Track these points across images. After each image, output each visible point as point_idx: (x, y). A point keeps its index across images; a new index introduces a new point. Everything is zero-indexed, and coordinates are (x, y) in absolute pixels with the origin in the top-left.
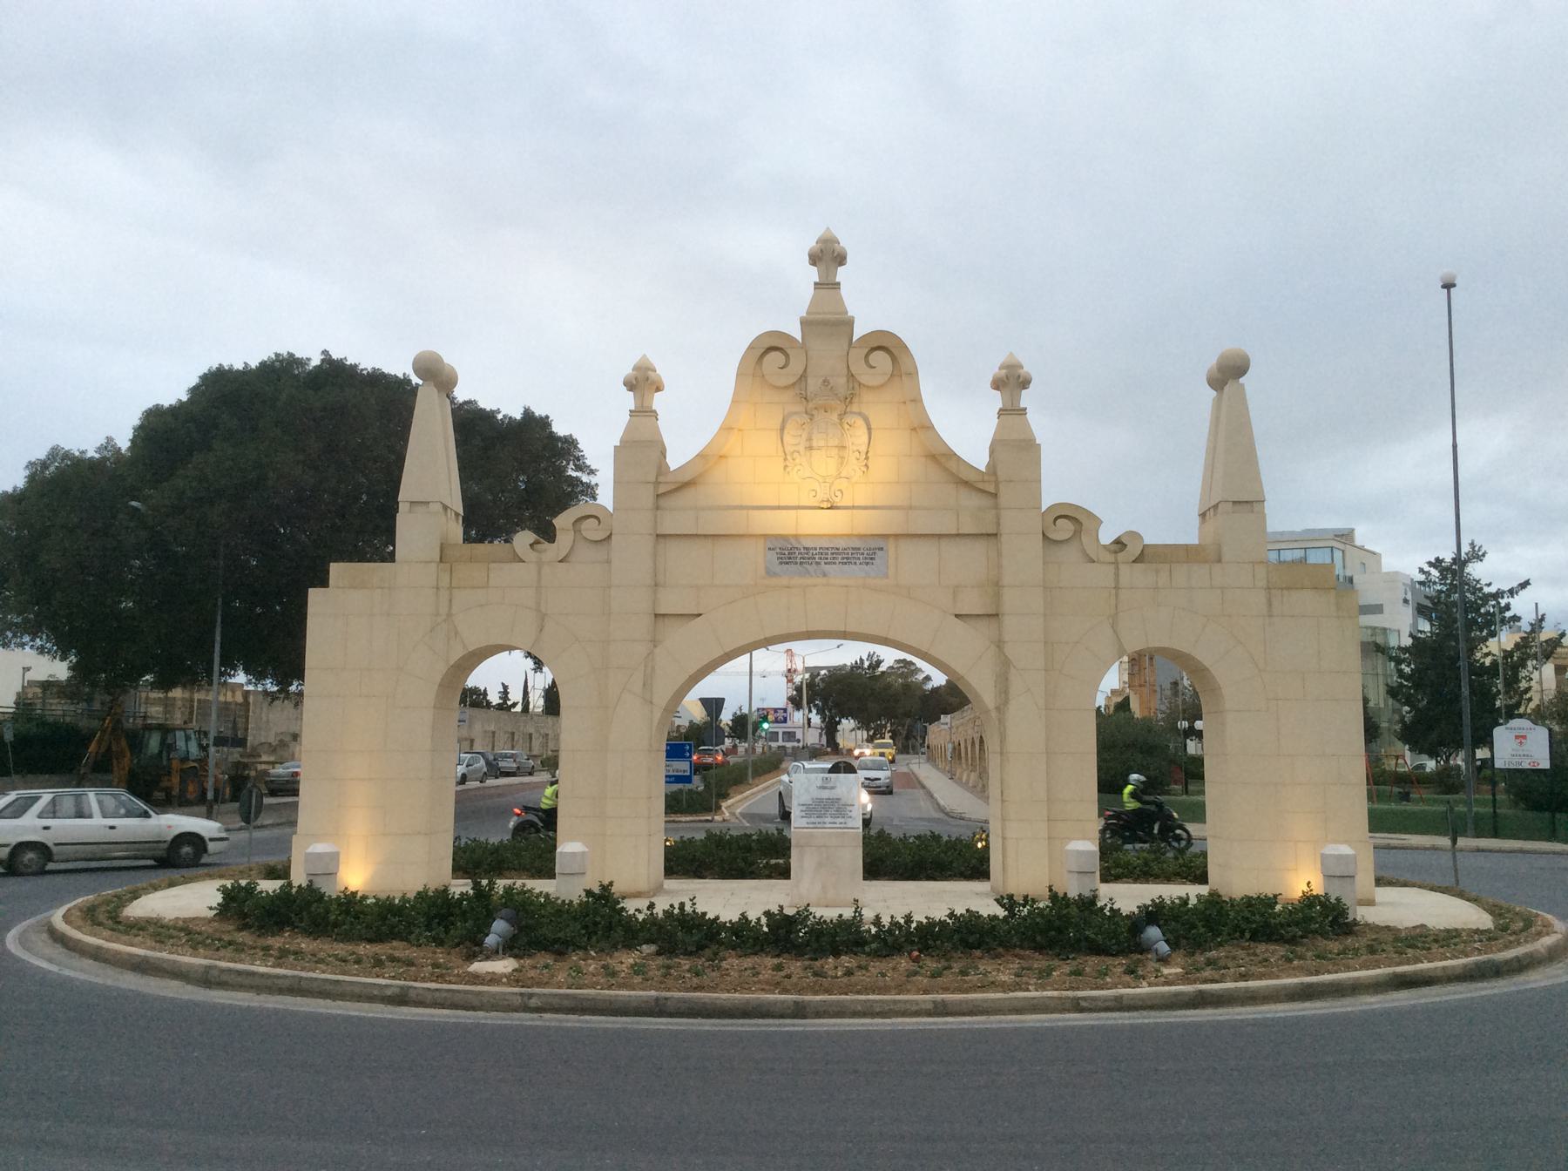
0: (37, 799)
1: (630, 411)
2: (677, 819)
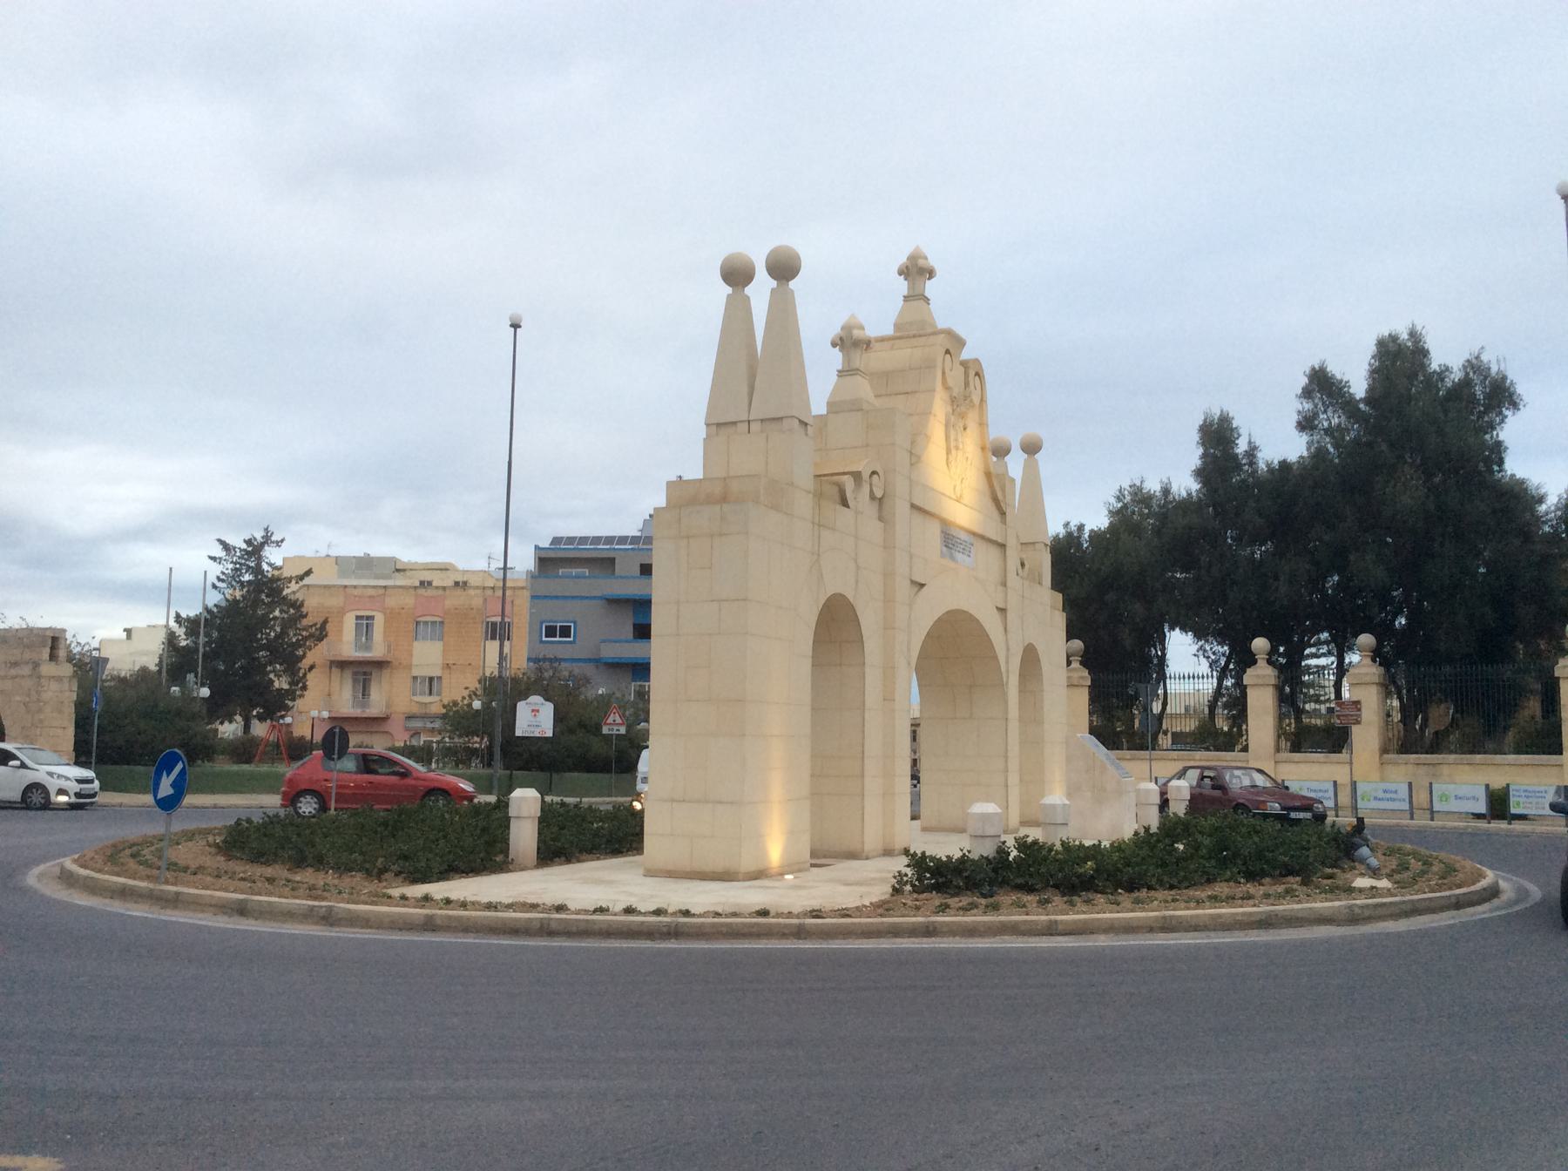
1: (838, 371)
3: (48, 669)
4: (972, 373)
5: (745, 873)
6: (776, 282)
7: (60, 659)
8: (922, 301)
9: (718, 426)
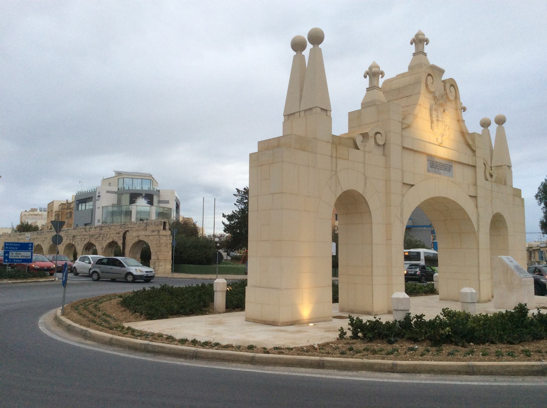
0: (121, 259)
2: (38, 280)
3: (163, 232)
4: (448, 85)
5: (282, 322)
6: (312, 45)
7: (166, 229)
8: (421, 54)
9: (288, 116)
